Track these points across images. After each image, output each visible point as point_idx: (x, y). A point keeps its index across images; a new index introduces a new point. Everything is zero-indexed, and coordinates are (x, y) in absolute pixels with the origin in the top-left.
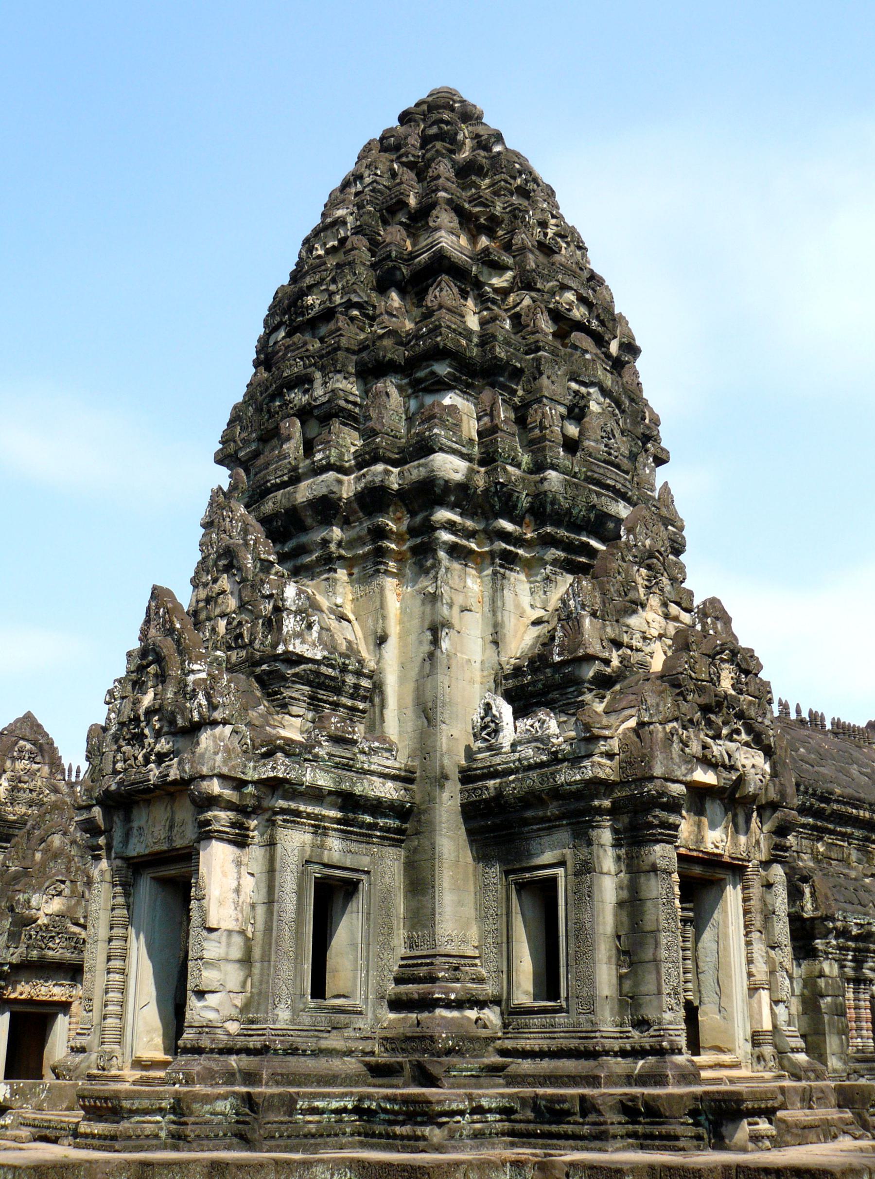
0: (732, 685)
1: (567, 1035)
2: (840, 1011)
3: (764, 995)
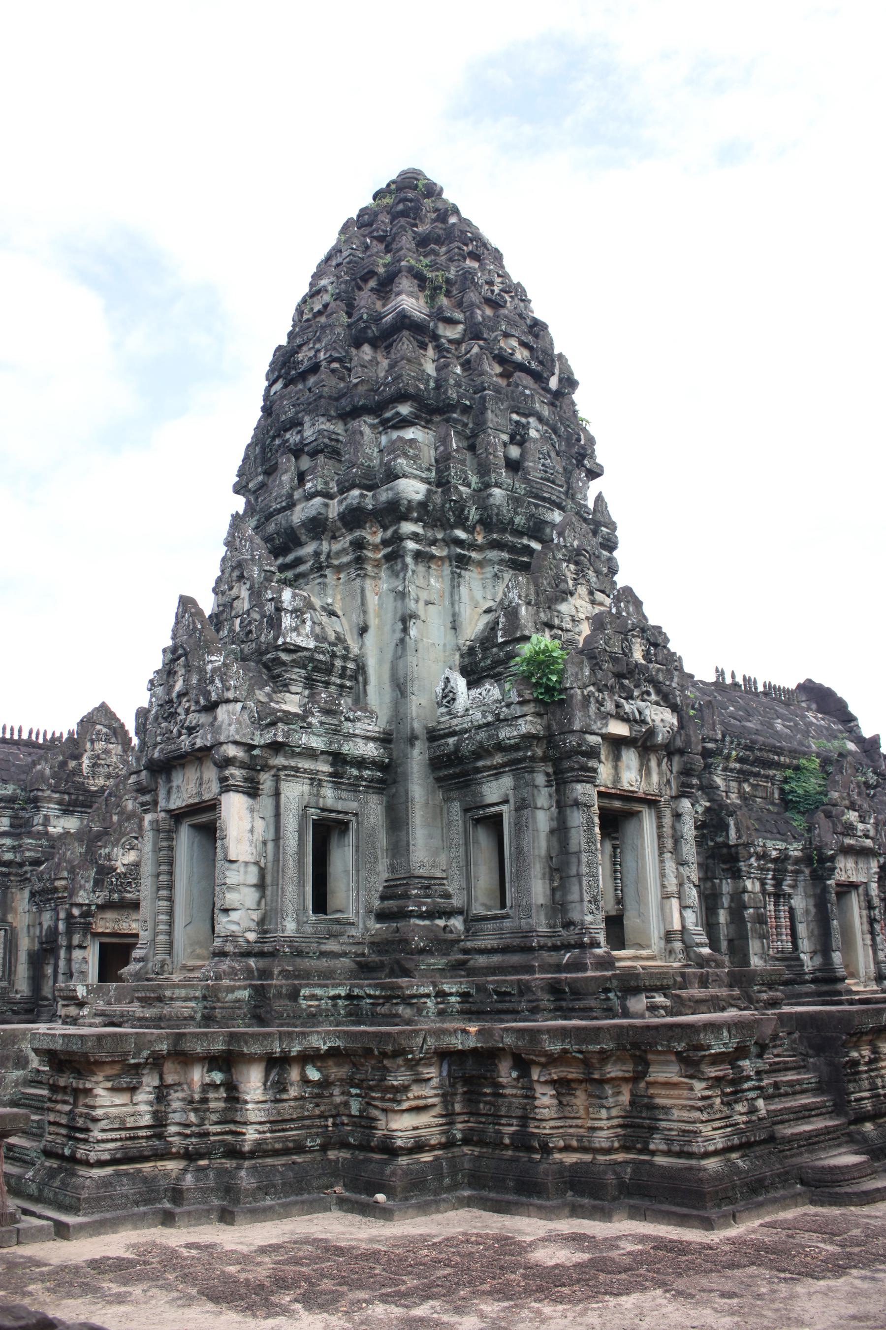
2: (761, 920)
3: (675, 902)
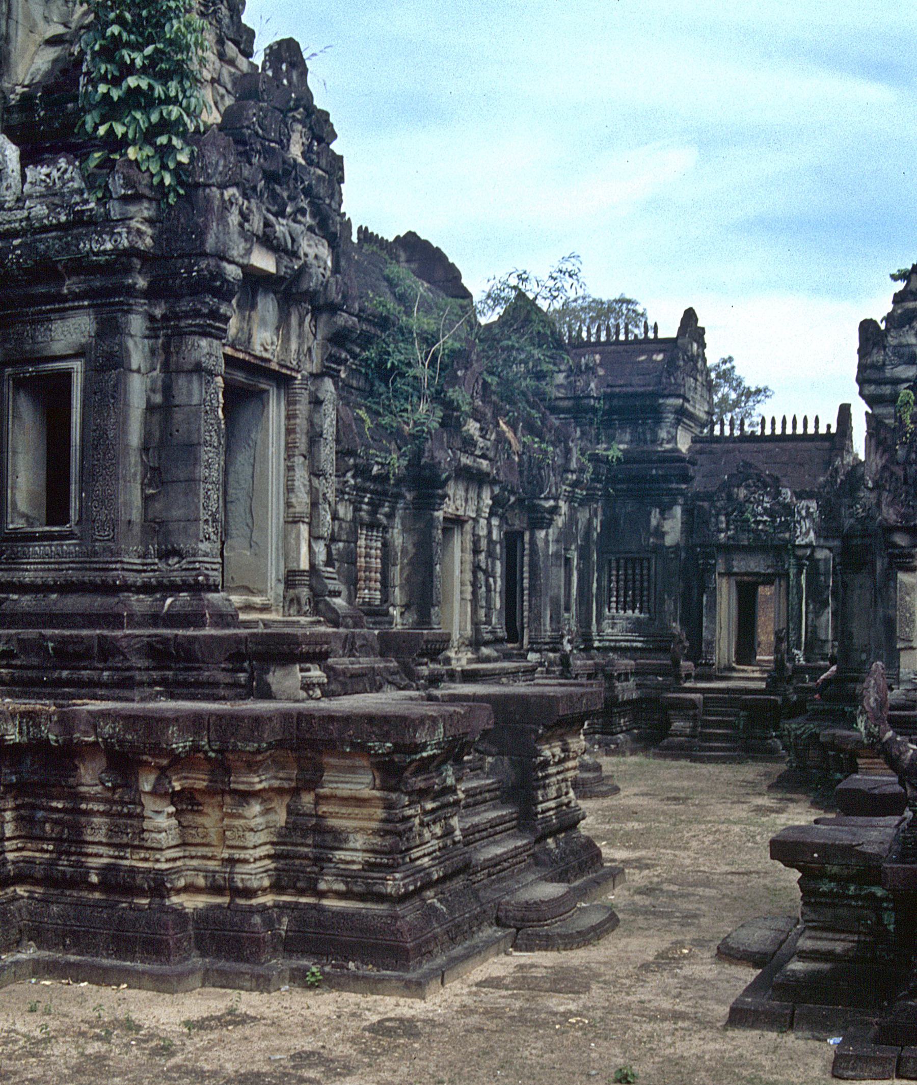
0: (302, 153)
1: (79, 566)
3: (304, 529)
